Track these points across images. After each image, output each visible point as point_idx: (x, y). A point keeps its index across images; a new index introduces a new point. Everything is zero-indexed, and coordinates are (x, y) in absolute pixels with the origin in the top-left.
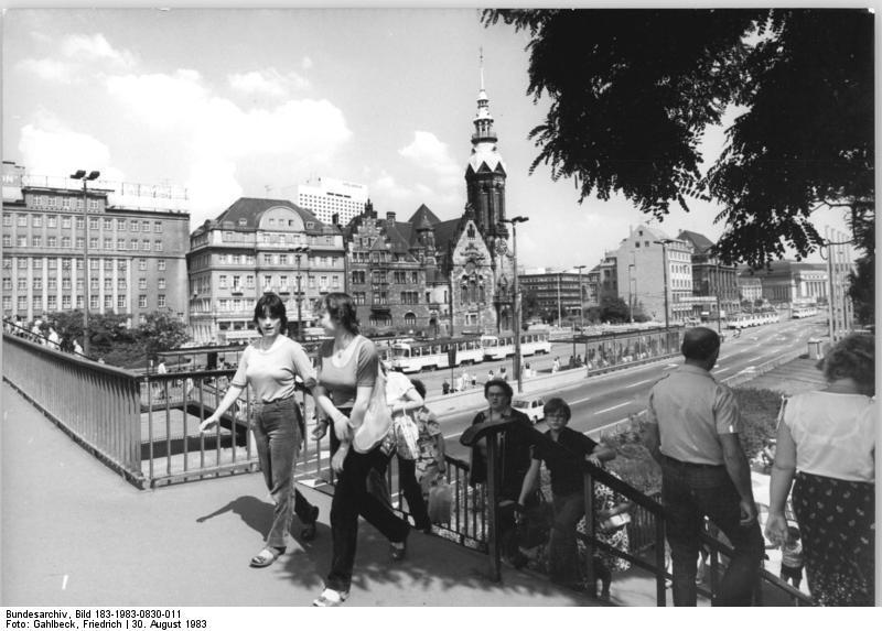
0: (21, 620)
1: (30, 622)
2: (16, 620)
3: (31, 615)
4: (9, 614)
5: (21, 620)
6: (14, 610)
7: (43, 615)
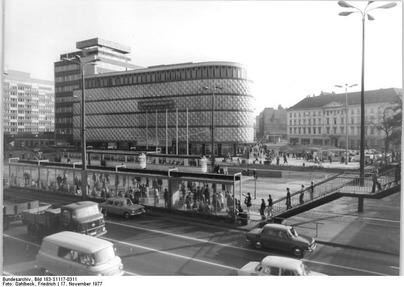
0: (10, 282)
1: (14, 282)
2: (7, 282)
3: (14, 280)
4: (4, 279)
5: (10, 282)
6: (7, 277)
7: (20, 280)
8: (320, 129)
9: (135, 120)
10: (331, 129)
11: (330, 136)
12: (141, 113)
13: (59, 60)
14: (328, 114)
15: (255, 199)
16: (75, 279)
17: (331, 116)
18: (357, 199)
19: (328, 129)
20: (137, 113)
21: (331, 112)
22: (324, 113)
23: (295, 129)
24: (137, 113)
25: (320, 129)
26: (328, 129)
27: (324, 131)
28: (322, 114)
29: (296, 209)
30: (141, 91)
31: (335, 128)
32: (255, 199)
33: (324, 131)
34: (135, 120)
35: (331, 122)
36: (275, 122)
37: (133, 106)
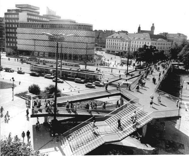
8: (119, 47)
9: (47, 44)
10: (124, 48)
11: (123, 51)
12: (50, 41)
13: (6, 12)
14: (123, 42)
15: (115, 58)
16: (153, 44)
17: (124, 43)
18: (111, 69)
19: (123, 48)
20: (48, 41)
21: (125, 41)
22: (122, 41)
23: (109, 46)
24: (48, 41)
25: (119, 47)
26: (123, 48)
27: (121, 48)
28: (121, 41)
29: (116, 145)
30: (49, 33)
31: (125, 48)
32: (115, 58)
33: (121, 48)
34: (47, 44)
35: (124, 45)
36: (99, 39)
37: (47, 38)
